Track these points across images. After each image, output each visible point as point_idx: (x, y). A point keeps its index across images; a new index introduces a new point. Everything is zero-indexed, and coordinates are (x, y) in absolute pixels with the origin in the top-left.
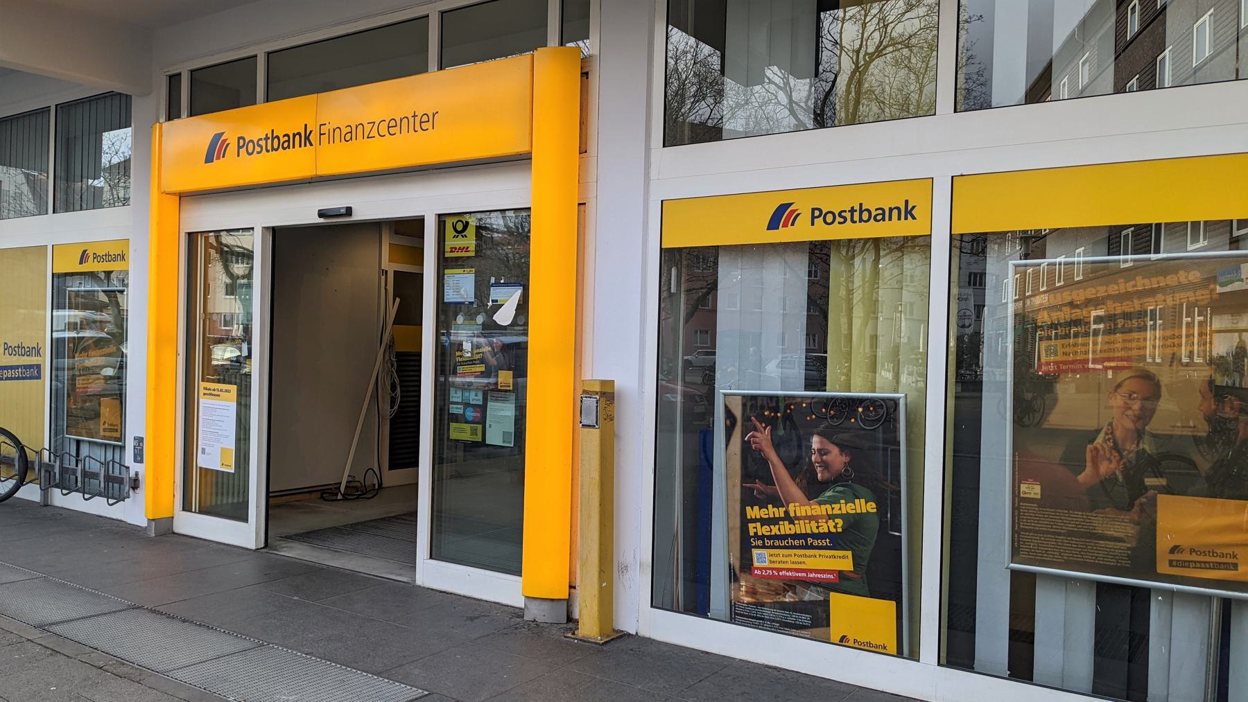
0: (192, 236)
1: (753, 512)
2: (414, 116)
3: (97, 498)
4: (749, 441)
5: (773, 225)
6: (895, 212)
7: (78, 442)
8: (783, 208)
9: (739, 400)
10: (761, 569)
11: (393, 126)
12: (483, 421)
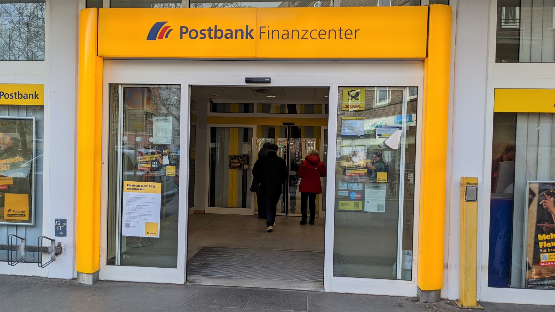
0: (113, 87)
1: (540, 237)
2: (340, 30)
3: (19, 263)
4: (542, 204)
5: (152, 36)
6: (239, 33)
7: (528, 284)
8: (158, 25)
9: (537, 185)
10: (544, 262)
11: (321, 34)
12: (362, 199)
